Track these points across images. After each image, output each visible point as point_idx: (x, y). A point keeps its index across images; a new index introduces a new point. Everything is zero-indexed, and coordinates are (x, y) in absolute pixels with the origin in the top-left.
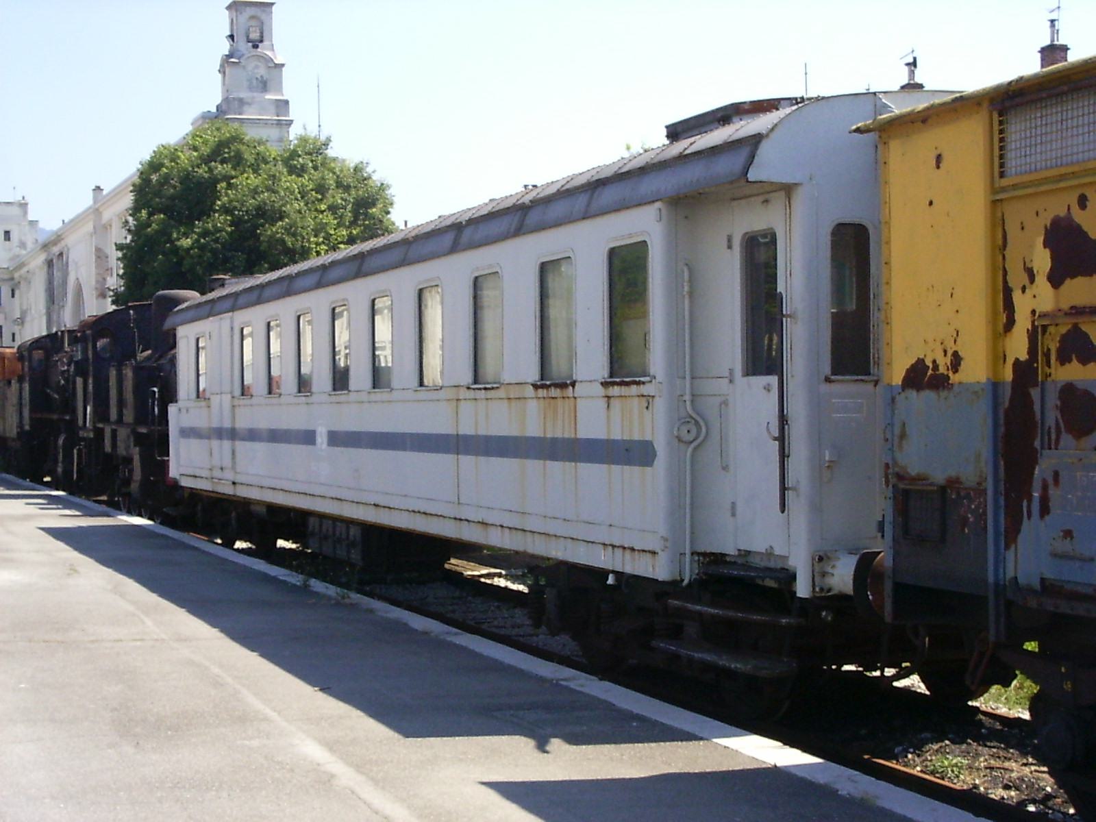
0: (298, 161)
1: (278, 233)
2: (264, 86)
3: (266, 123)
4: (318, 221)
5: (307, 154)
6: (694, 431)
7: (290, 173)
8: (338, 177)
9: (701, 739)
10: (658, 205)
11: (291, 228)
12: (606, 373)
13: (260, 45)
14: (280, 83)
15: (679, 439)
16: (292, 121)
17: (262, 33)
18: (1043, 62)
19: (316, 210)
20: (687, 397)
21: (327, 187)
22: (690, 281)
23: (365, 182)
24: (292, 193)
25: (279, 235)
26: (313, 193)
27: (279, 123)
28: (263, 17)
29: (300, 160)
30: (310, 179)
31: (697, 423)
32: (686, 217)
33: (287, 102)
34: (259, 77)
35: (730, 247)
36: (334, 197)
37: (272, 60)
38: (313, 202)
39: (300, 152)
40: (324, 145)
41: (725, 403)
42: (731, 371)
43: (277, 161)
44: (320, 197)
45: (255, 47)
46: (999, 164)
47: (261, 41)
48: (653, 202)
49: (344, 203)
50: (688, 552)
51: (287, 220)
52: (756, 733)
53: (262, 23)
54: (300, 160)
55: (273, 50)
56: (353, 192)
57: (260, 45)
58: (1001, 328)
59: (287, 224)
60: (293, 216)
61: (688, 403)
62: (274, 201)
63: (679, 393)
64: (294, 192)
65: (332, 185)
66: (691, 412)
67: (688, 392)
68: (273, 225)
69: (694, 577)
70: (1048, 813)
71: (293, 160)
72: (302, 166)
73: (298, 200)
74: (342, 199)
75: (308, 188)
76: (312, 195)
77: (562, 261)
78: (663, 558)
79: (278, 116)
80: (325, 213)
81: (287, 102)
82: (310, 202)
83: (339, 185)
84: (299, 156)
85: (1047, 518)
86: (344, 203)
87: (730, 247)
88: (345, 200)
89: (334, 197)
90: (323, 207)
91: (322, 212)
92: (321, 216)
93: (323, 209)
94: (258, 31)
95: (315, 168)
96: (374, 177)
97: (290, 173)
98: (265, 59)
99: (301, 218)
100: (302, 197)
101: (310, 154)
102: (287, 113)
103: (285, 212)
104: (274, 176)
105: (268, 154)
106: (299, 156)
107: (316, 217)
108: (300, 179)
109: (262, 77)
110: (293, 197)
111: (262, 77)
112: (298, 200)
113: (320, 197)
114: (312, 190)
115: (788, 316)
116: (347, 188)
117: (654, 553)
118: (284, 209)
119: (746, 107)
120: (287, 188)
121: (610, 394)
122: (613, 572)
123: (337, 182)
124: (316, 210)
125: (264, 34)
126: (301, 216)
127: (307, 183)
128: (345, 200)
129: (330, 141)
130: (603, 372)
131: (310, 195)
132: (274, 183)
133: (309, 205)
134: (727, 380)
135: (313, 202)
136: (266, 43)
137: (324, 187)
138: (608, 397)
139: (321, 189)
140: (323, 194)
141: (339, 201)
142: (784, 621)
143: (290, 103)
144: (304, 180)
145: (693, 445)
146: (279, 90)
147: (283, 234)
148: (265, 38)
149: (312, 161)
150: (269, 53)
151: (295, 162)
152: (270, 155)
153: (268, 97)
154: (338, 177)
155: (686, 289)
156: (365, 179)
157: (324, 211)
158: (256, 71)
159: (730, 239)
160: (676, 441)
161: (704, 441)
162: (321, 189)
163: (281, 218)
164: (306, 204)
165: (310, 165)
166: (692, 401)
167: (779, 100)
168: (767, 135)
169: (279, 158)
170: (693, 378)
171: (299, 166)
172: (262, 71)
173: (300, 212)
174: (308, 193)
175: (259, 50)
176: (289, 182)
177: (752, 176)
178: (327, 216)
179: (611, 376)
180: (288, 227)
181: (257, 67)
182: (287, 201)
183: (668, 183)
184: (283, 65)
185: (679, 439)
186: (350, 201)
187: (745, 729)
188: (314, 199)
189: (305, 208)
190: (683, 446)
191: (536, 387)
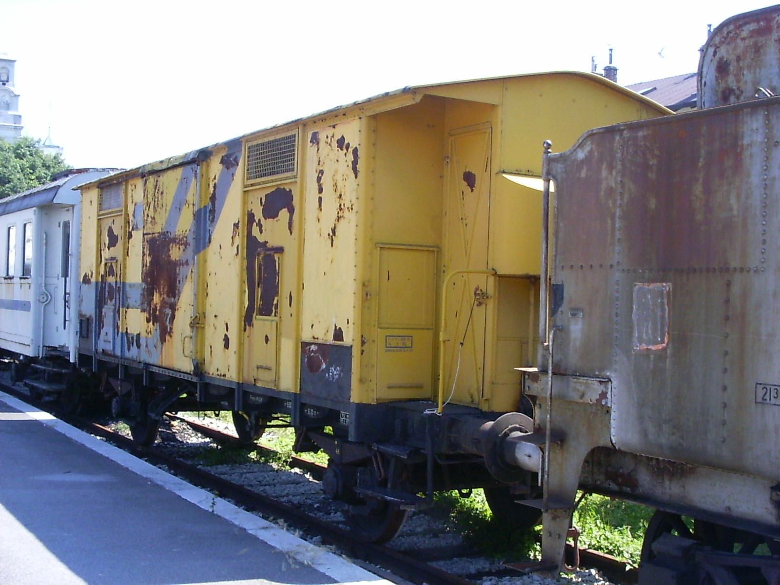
0: (21, 151)
1: (6, 190)
2: (8, 106)
3: (7, 127)
4: (30, 185)
5: (26, 147)
6: (46, 298)
7: (16, 157)
8: (44, 161)
9: (21, 412)
10: (35, 208)
11: (14, 188)
12: (22, 274)
13: (7, 83)
14: (17, 105)
15: (39, 300)
16: (22, 127)
17: (8, 78)
18: (142, 168)
19: (29, 179)
20: (43, 285)
21: (36, 166)
22: (46, 239)
23: (59, 165)
24: (16, 168)
25: (7, 192)
26: (28, 169)
27: (15, 128)
28: (10, 68)
29: (22, 150)
30: (27, 161)
31: (47, 295)
32: (46, 214)
33: (20, 116)
34: (5, 101)
35: (59, 226)
36: (40, 172)
37: (13, 92)
38: (28, 174)
39: (23, 146)
40: (37, 142)
41: (57, 287)
42: (58, 276)
43: (10, 149)
44: (31, 171)
45: (4, 84)
46: (100, 207)
47: (7, 81)
48: (33, 207)
49: (45, 176)
50: (41, 346)
51: (12, 183)
52: (45, 411)
53: (9, 71)
54: (22, 150)
55: (14, 87)
56: (52, 170)
57: (7, 83)
58: (99, 263)
59: (12, 186)
60: (15, 181)
61: (43, 287)
62: (5, 173)
63: (40, 283)
64: (17, 168)
65: (39, 165)
66: (45, 291)
67: (43, 282)
68: (4, 186)
69: (44, 355)
70: (572, 579)
71: (18, 150)
72: (23, 154)
73: (19, 173)
74: (44, 173)
75: (26, 166)
76: (27, 170)
77: (548, 183)
78: (31, 348)
79: (15, 124)
80: (34, 181)
81: (20, 116)
82: (26, 174)
83: (44, 165)
84: (22, 148)
85: (138, 332)
86: (45, 176)
87: (59, 226)
88: (46, 174)
89: (40, 172)
90: (33, 177)
91: (33, 180)
92: (31, 182)
93: (33, 178)
94: (6, 76)
95: (31, 155)
96: (65, 162)
97: (16, 157)
98: (9, 91)
99: (20, 183)
100: (22, 172)
101: (29, 147)
102: (20, 122)
103: (11, 179)
104: (6, 158)
105: (4, 146)
106: (22, 148)
107: (29, 183)
108: (22, 161)
109: (7, 101)
110: (16, 171)
111: (7, 101)
112: (19, 173)
113: (31, 171)
114: (28, 167)
115: (70, 255)
116: (48, 168)
117: (29, 346)
118: (10, 177)
119: (75, 171)
120: (13, 166)
121: (22, 282)
122: (23, 355)
123: (43, 164)
124: (29, 179)
125: (10, 78)
126: (20, 181)
127: (25, 164)
128: (46, 174)
129: (41, 140)
130: (20, 274)
131: (26, 171)
132: (6, 162)
133: (26, 176)
134: (57, 279)
135: (28, 174)
136: (10, 82)
137: (35, 166)
138: (21, 284)
139: (33, 167)
140: (33, 170)
141: (43, 174)
142: (64, 371)
143: (22, 118)
144: (24, 162)
145: (45, 303)
146: (16, 109)
147: (8, 191)
148: (9, 80)
149: (29, 151)
150: (12, 89)
151: (19, 151)
152: (5, 147)
153: (11, 113)
154: (44, 161)
155: (44, 242)
156: (59, 163)
157: (34, 179)
158: (3, 98)
159: (59, 223)
160: (38, 302)
161: (49, 302)
162: (33, 167)
163: (9, 182)
164: (24, 176)
165: (28, 153)
166: (45, 286)
167: (89, 169)
168: (62, 186)
169: (12, 148)
170: (46, 277)
171: (21, 154)
172: (7, 98)
173: (19, 179)
174: (25, 169)
175: (6, 86)
176: (15, 162)
177: (55, 201)
178: (35, 182)
179: (23, 275)
180: (12, 187)
181: (4, 96)
182: (13, 173)
183: (36, 200)
184: (19, 96)
185: (39, 300)
186: (49, 175)
187: (38, 408)
188: (28, 173)
189: (23, 177)
190: (41, 304)
191: (5, 278)
